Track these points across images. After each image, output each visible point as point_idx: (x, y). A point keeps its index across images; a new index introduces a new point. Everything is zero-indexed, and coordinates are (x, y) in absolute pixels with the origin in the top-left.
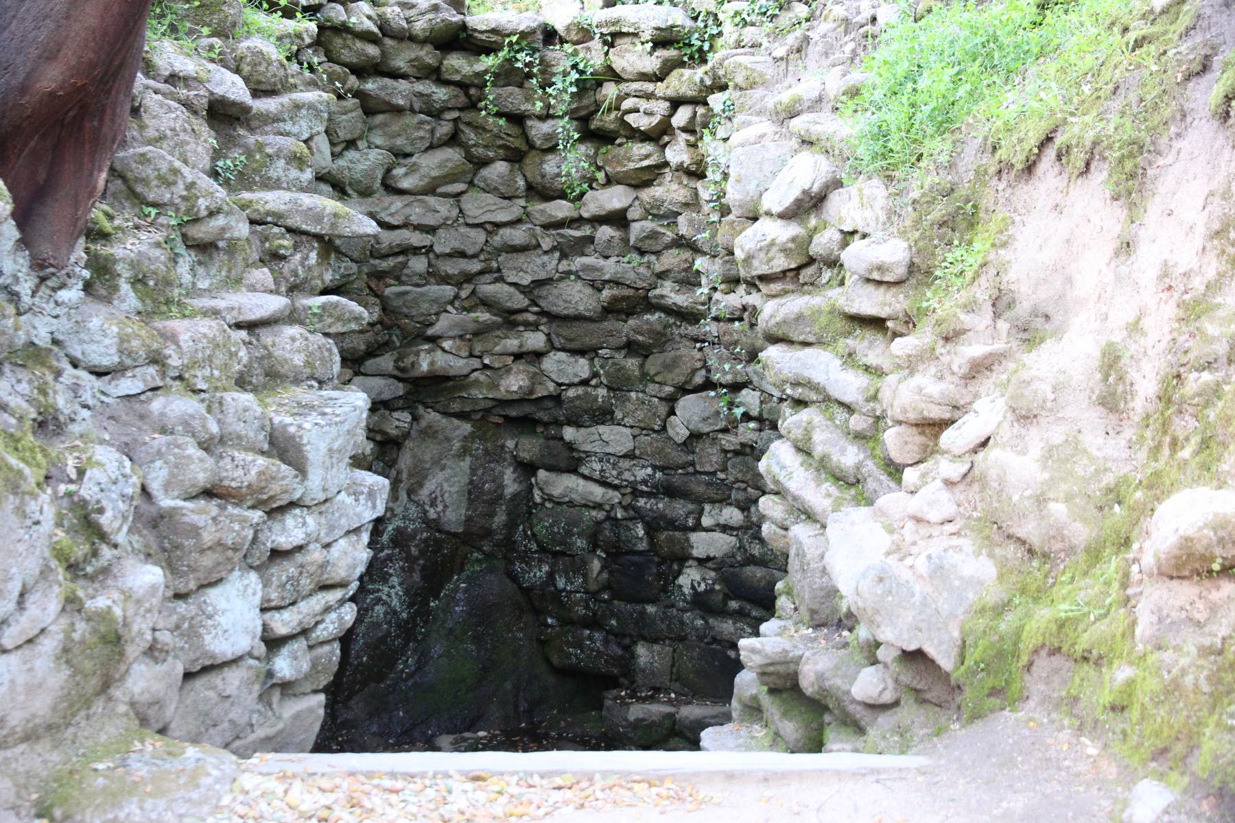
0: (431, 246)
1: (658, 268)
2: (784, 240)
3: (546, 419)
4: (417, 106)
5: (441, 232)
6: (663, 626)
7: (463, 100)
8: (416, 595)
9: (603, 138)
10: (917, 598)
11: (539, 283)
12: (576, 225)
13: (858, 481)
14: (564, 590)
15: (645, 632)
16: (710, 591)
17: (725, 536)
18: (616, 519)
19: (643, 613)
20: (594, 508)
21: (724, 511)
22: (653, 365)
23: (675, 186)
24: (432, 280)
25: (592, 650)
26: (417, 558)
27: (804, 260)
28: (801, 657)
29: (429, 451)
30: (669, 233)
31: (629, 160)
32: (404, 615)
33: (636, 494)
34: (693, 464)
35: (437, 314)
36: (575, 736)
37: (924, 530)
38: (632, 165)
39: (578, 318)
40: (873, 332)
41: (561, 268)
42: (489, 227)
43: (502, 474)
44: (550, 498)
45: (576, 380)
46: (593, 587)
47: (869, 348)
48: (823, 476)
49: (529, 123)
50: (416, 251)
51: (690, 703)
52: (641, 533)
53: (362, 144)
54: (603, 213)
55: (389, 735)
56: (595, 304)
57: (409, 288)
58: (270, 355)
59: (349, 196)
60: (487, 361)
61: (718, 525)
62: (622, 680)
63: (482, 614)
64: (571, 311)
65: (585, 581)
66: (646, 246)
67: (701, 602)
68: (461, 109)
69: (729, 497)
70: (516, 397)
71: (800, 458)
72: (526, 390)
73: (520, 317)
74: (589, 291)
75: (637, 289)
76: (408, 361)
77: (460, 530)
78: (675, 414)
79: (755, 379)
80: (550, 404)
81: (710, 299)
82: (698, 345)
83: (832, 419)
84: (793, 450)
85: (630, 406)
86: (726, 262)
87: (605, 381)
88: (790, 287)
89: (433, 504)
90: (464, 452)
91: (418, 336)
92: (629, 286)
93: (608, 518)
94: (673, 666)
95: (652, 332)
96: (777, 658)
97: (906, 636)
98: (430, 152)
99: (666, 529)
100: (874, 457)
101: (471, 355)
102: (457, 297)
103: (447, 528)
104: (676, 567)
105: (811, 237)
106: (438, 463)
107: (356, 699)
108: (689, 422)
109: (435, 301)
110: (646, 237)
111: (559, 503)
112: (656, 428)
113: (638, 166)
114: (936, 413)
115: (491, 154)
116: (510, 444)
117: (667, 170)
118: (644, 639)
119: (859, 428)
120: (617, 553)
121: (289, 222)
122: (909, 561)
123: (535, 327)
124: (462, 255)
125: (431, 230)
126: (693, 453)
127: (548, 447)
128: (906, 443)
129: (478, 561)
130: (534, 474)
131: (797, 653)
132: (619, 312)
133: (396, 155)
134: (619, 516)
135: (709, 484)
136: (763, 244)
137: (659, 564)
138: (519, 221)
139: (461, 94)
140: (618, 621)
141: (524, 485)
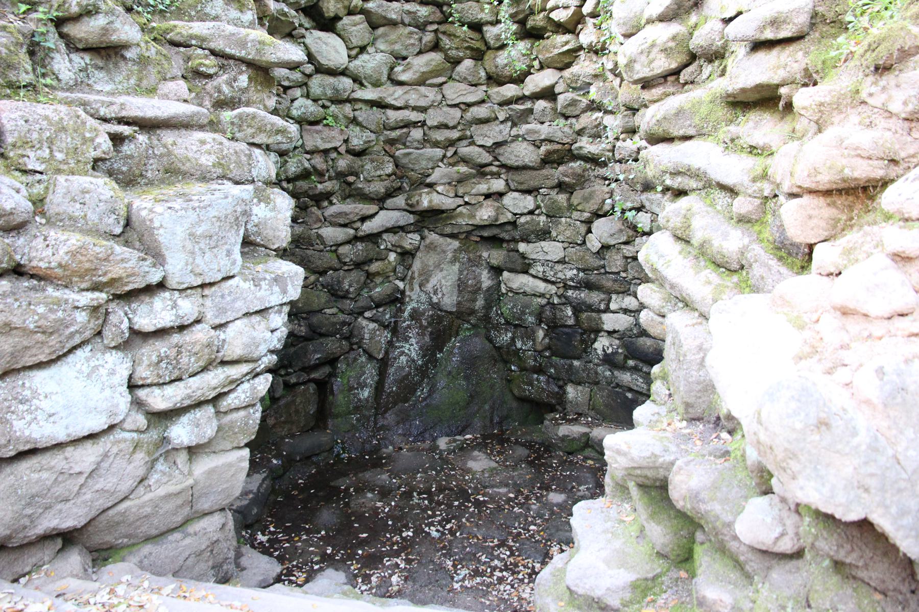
0: (425, 121)
1: (578, 127)
2: (665, 39)
3: (507, 238)
4: (407, 21)
5: (430, 111)
6: (584, 375)
7: (438, 16)
8: (427, 350)
9: (533, 35)
10: (863, 438)
11: (498, 145)
12: (521, 102)
13: (742, 267)
14: (521, 349)
15: (573, 378)
16: (615, 353)
17: (626, 316)
18: (553, 304)
19: (571, 365)
20: (540, 296)
21: (626, 299)
22: (576, 199)
23: (587, 63)
24: (428, 145)
25: (539, 387)
26: (427, 327)
27: (683, 58)
28: (672, 464)
29: (432, 259)
30: (584, 100)
31: (554, 47)
32: (420, 362)
33: (566, 287)
34: (604, 267)
35: (433, 168)
36: (526, 442)
37: (855, 326)
38: (556, 51)
39: (525, 168)
40: (759, 113)
41: (513, 133)
42: (463, 107)
43: (480, 274)
44: (511, 290)
45: (526, 211)
46: (539, 348)
47: (755, 128)
48: (702, 263)
49: (485, 28)
50: (415, 124)
51: (600, 425)
52: (570, 313)
53: (370, 49)
54: (538, 90)
55: (410, 435)
56: (536, 157)
57: (411, 150)
58: (169, 153)
59: (365, 86)
60: (466, 199)
61: (621, 309)
62: (557, 407)
63: (470, 362)
64: (520, 163)
65: (534, 344)
66: (568, 112)
67: (609, 360)
68: (439, 23)
69: (629, 289)
70: (486, 223)
71: (679, 246)
72: (493, 218)
73: (488, 169)
74: (532, 148)
75: (564, 144)
76: (414, 200)
77: (454, 310)
78: (591, 232)
79: (647, 204)
80: (509, 228)
81: (614, 146)
82: (607, 182)
83: (713, 205)
84: (671, 239)
85: (561, 228)
86: (625, 116)
87: (544, 211)
88: (672, 90)
89: (435, 293)
90: (455, 260)
91: (421, 184)
92: (558, 143)
93: (548, 303)
94: (590, 400)
95: (574, 174)
96: (645, 464)
97: (841, 498)
98: (421, 55)
99: (586, 311)
100: (761, 241)
101: (456, 196)
102: (444, 156)
103: (445, 308)
104: (592, 336)
105: (691, 34)
106: (438, 266)
107: (390, 412)
108: (601, 237)
109: (430, 159)
110: (569, 105)
111: (517, 293)
112: (579, 242)
113: (561, 51)
114: (863, 171)
115: (461, 54)
116: (485, 254)
117: (582, 53)
118: (572, 382)
119: (743, 211)
120: (554, 326)
121: (212, 45)
122: (842, 375)
123: (497, 175)
124: (446, 127)
125: (423, 110)
126: (604, 259)
127: (509, 256)
128: (810, 217)
129: (467, 329)
130: (501, 275)
131: (669, 458)
132: (552, 162)
133: (396, 58)
134: (556, 302)
135: (615, 281)
136: (643, 47)
137: (582, 334)
138: (483, 101)
139: (438, 11)
140: (555, 370)
141: (495, 282)
